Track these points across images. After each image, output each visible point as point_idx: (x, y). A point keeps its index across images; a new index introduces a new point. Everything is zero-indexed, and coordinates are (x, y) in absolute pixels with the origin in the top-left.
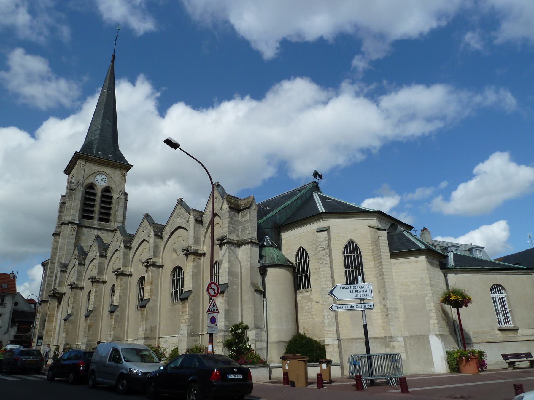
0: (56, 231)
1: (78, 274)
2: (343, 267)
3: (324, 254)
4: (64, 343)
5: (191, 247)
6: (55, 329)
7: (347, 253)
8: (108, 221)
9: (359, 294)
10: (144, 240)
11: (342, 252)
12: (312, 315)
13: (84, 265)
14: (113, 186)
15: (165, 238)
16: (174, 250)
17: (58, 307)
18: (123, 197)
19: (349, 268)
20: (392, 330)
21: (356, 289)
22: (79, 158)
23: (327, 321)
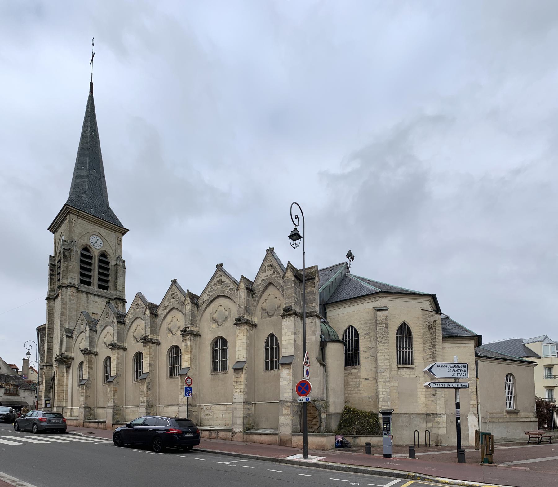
0: (49, 295)
1: (90, 340)
2: (395, 348)
3: (384, 333)
4: (84, 406)
5: (243, 317)
7: (400, 334)
8: (106, 288)
9: (456, 373)
10: (173, 308)
11: (395, 333)
12: (360, 390)
14: (109, 251)
18: (121, 264)
19: (400, 349)
20: (438, 408)
21: (454, 368)
23: (383, 396)
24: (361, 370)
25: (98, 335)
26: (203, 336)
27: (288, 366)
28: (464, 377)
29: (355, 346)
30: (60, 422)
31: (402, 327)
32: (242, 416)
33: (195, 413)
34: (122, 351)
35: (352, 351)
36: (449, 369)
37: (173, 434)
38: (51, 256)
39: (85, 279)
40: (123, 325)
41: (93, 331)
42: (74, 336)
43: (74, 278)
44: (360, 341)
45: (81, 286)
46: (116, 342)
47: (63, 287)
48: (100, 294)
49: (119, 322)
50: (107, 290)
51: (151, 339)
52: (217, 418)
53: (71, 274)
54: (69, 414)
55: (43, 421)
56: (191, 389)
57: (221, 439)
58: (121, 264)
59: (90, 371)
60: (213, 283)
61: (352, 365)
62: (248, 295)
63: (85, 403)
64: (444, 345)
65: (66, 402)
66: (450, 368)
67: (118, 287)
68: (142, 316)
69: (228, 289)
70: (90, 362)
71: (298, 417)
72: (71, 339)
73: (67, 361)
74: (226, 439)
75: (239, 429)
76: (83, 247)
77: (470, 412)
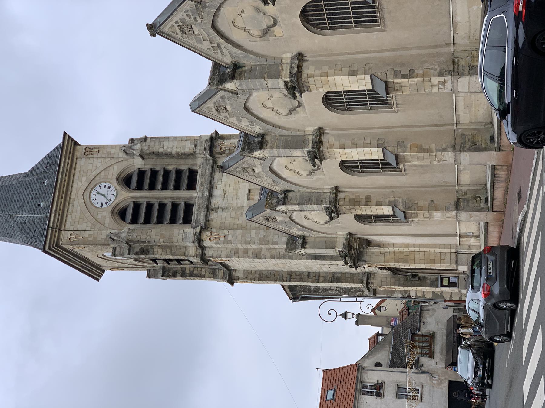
0: (223, 278)
1: (307, 203)
4: (454, 213)
6: (424, 246)
8: (193, 174)
10: (290, 218)
13: (286, 192)
14: (116, 170)
15: (287, 187)
16: (266, 32)
17: (379, 245)
18: (138, 146)
22: (57, 245)
25: (293, 188)
30: (491, 258)
34: (325, 138)
38: (149, 276)
40: (267, 138)
41: (286, 197)
42: (300, 233)
43: (182, 235)
45: (197, 221)
46: (306, 150)
47: (203, 254)
48: (206, 186)
49: (262, 145)
50: (196, 172)
51: (291, 76)
53: (175, 240)
54: (472, 241)
55: (490, 290)
58: (138, 146)
59: (374, 201)
63: (447, 209)
65: (446, 246)
67: (187, 150)
68: (242, 99)
70: (355, 202)
72: (308, 240)
73: (356, 246)
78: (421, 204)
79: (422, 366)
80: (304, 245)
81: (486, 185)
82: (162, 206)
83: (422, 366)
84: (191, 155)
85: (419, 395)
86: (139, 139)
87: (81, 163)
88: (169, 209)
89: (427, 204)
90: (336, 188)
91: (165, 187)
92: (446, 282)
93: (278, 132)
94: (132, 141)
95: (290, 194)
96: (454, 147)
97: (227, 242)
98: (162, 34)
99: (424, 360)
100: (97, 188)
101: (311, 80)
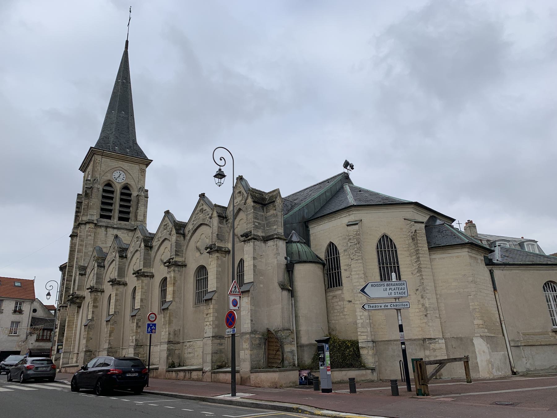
0: (73, 232)
1: (97, 277)
2: (377, 264)
3: (356, 249)
4: (84, 350)
6: (75, 335)
8: (127, 220)
10: (165, 239)
12: (345, 315)
14: (132, 183)
15: (106, 268)
16: (198, 249)
18: (143, 194)
19: (383, 264)
21: (391, 287)
22: (94, 154)
24: (345, 291)
25: (106, 270)
26: (188, 266)
27: (246, 294)
28: (403, 295)
29: (337, 266)
30: (49, 369)
31: (384, 240)
32: (211, 352)
33: (177, 352)
34: (122, 287)
35: (335, 270)
36: (385, 288)
37: (113, 374)
38: (78, 195)
39: (106, 214)
40: (125, 259)
41: (101, 267)
42: (87, 273)
43: (94, 214)
44: (341, 258)
45: (101, 221)
46: (117, 278)
47: (82, 224)
48: (119, 226)
49: (121, 257)
51: (144, 272)
52: (198, 356)
53: (91, 210)
54: (75, 360)
55: (30, 369)
56: (155, 325)
57: (193, 380)
58: (143, 194)
59: (95, 310)
60: (197, 212)
61: (337, 286)
62: (221, 222)
63: (86, 346)
64: (433, 256)
65: (74, 346)
66: (386, 287)
67: (138, 217)
69: (208, 217)
70: (95, 300)
71: (262, 352)
72: (83, 277)
73: (78, 301)
74: (198, 380)
75: (208, 368)
76: (105, 183)
77: (476, 335)
78: (91, 333)
79: (31, 335)
80: (81, 275)
81: (183, 366)
82: (111, 204)
83: (31, 335)
84: (136, 220)
85: (13, 334)
86: (147, 194)
87: (137, 167)
88: (109, 207)
89: (90, 336)
90: (103, 291)
91: (121, 206)
92: (59, 347)
93: (127, 264)
94: (147, 191)
95: (103, 269)
96: (111, 348)
97: (87, 236)
98: (165, 216)
99: (35, 337)
100: (123, 174)
101: (141, 281)
